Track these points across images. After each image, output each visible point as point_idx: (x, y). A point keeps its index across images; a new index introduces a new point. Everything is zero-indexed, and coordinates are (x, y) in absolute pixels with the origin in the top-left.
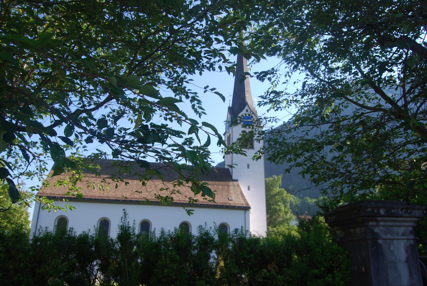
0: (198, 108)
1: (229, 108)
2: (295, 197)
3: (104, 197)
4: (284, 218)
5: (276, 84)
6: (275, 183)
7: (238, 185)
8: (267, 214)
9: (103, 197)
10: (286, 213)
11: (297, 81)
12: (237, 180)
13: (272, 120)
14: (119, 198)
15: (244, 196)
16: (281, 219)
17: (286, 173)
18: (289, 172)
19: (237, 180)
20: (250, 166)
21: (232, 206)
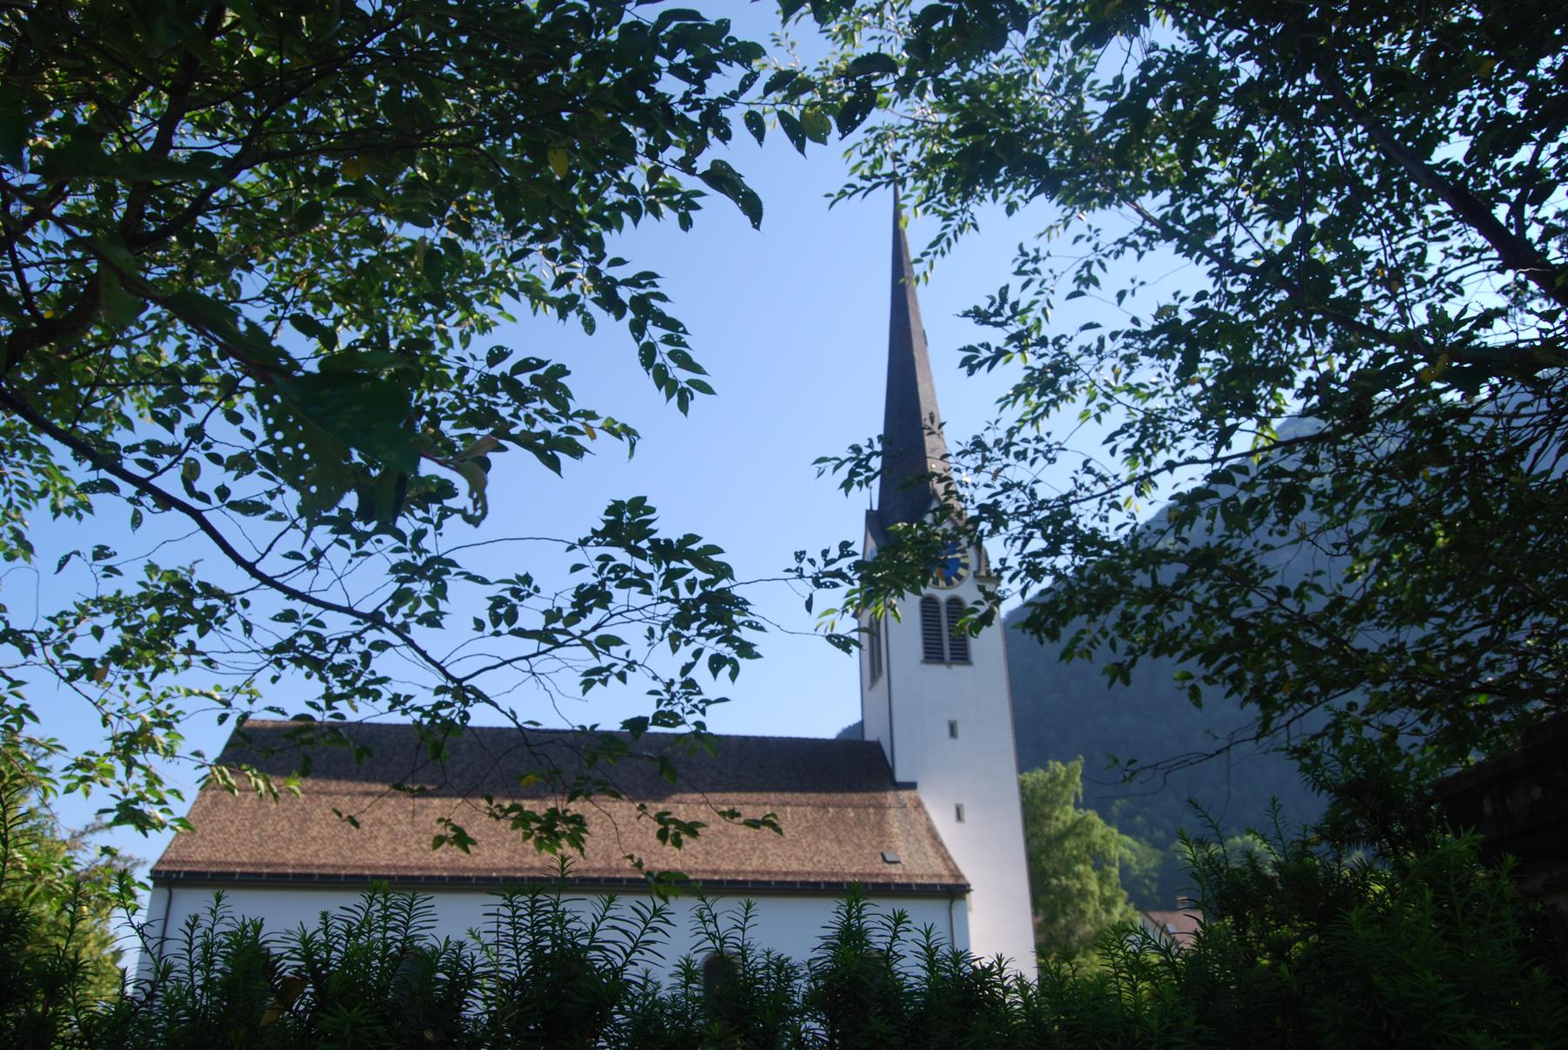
0: (670, 363)
1: (870, 515)
2: (1136, 845)
3: (411, 868)
4: (1100, 923)
5: (1039, 320)
6: (1059, 789)
7: (919, 805)
8: (1035, 914)
9: (405, 867)
10: (1108, 904)
11: (1129, 287)
12: (912, 786)
13: (1030, 454)
14: (465, 869)
15: (941, 844)
16: (1089, 928)
17: (1111, 685)
18: (1127, 682)
19: (912, 786)
20: (960, 730)
21: (897, 885)
